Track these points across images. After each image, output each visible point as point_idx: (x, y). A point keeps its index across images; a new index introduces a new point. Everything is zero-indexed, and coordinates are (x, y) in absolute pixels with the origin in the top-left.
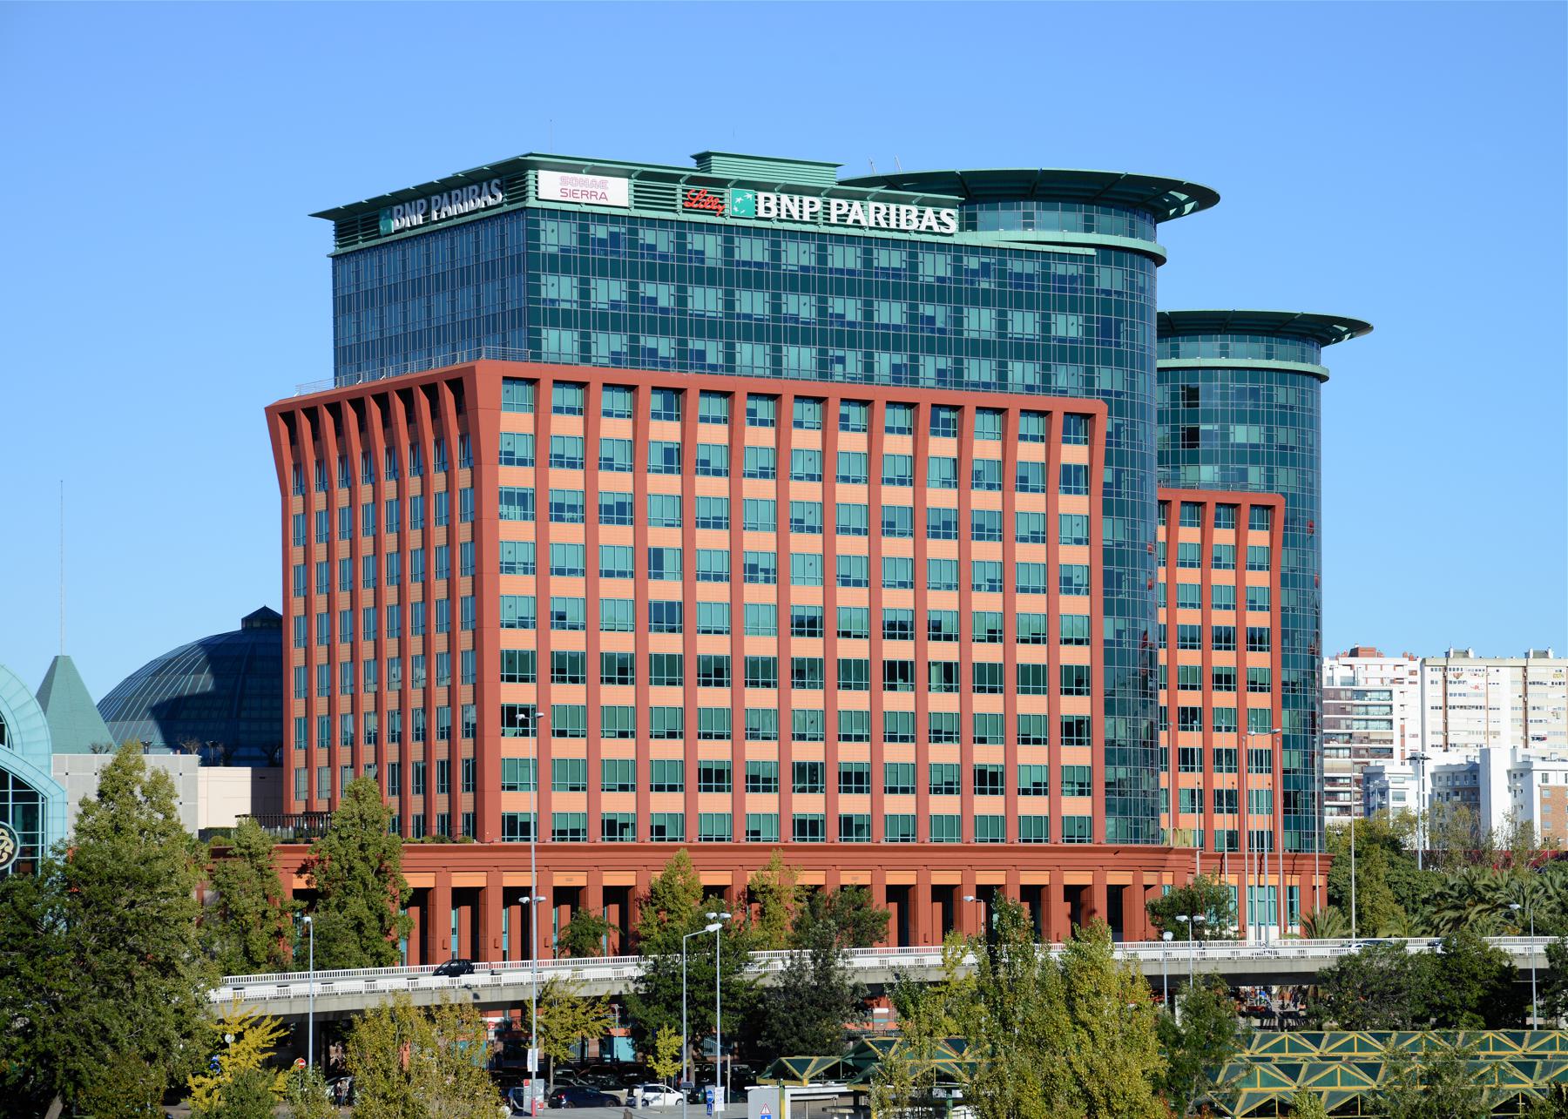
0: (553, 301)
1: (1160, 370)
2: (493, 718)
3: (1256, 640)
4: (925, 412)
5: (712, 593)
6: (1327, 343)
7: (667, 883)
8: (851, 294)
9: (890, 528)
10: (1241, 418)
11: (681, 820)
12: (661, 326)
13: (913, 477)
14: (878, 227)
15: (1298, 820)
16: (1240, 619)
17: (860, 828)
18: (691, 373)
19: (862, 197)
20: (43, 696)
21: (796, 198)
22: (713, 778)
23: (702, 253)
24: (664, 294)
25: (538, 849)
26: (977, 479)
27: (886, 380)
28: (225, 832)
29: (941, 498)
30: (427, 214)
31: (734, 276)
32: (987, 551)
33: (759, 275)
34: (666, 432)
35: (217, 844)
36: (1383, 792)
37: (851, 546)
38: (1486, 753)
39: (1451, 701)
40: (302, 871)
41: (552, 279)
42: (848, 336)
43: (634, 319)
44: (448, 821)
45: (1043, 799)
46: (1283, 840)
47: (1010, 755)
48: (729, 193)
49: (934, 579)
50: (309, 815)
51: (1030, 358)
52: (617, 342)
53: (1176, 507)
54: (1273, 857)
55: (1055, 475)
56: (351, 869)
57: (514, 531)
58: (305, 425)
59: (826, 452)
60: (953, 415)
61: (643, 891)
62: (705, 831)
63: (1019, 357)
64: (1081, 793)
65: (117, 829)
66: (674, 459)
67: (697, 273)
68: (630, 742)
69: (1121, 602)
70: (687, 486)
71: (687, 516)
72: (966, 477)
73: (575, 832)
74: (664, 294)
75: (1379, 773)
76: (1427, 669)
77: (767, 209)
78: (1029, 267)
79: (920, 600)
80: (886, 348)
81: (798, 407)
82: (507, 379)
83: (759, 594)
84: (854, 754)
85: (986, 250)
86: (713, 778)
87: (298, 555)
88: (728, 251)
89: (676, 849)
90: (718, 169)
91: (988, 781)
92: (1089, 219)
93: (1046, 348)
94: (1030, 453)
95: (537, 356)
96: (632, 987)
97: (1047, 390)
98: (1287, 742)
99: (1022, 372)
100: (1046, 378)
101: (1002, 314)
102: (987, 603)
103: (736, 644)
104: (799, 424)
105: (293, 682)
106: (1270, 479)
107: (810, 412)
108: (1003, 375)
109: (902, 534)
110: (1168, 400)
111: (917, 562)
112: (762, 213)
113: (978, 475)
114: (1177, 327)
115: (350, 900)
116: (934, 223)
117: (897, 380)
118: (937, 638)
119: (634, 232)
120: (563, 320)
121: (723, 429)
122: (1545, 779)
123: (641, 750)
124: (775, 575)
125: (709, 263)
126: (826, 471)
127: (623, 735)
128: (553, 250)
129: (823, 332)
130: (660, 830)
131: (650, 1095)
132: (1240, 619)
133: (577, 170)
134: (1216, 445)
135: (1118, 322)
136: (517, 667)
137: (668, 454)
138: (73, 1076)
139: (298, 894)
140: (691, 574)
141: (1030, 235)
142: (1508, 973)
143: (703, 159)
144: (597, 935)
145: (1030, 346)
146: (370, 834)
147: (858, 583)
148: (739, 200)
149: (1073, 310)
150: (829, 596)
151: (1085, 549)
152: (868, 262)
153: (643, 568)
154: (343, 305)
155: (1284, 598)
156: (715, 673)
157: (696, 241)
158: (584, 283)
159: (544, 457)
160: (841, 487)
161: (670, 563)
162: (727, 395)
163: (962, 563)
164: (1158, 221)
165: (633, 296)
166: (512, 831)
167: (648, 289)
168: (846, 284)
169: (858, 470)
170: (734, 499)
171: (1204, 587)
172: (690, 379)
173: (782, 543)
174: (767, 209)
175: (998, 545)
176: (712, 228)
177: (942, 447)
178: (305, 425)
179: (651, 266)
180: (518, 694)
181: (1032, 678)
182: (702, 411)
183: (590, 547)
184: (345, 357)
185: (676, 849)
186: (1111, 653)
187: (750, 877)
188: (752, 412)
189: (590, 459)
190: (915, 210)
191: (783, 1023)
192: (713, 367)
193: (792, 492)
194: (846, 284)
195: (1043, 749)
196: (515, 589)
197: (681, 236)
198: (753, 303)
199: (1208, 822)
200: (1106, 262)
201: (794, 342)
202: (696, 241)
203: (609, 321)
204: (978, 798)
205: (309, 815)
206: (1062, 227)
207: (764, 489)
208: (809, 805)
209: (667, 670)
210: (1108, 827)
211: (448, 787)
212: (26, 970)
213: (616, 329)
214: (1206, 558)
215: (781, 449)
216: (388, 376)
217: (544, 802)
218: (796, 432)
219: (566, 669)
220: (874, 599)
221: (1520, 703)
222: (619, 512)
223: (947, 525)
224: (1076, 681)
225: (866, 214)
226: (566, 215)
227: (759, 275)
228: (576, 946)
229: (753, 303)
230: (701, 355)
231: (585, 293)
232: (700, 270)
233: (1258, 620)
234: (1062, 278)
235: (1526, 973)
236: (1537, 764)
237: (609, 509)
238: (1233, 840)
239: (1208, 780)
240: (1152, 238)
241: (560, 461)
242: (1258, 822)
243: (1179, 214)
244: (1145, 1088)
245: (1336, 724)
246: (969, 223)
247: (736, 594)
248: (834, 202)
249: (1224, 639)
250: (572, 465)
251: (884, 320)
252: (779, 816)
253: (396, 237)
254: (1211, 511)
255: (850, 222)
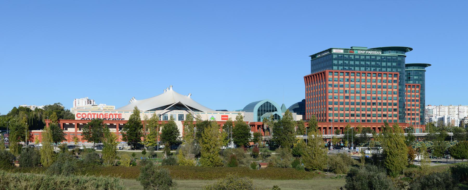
0: (334, 63)
1: (406, 70)
2: (328, 109)
3: (417, 101)
4: (377, 74)
5: (352, 95)
6: (426, 67)
7: (347, 127)
8: (369, 61)
9: (373, 87)
10: (415, 76)
11: (349, 120)
12: (347, 65)
13: (376, 81)
15: (422, 121)
16: (415, 98)
17: (369, 121)
18: (350, 71)
19: (370, 51)
20: (281, 108)
22: (352, 115)
23: (351, 57)
24: (347, 62)
25: (332, 123)
26: (384, 82)
27: (373, 71)
28: (299, 121)
29: (379, 84)
30: (321, 55)
31: (355, 60)
32: (385, 90)
33: (358, 60)
34: (347, 77)
35: (298, 122)
36: (432, 121)
38: (444, 116)
39: (440, 111)
40: (307, 125)
41: (334, 61)
42: (368, 66)
43: (344, 65)
44: (323, 120)
45: (391, 118)
46: (420, 123)
47: (387, 113)
48: (354, 51)
49: (378, 93)
50: (308, 119)
51: (390, 68)
52: (342, 68)
53: (407, 86)
54: (419, 125)
55: (393, 81)
56: (312, 125)
57: (330, 88)
58: (308, 78)
59: (366, 79)
60: (381, 75)
61: (344, 128)
62: (351, 121)
63: (389, 68)
64: (396, 117)
65: (287, 118)
66: (348, 80)
67: (350, 59)
68: (343, 111)
69: (401, 95)
70: (350, 83)
71: (350, 86)
72: (382, 81)
73: (337, 121)
74: (347, 62)
75: (431, 119)
76: (437, 107)
78: (390, 58)
79: (377, 95)
80: (373, 67)
81: (362, 74)
82: (329, 72)
83: (358, 95)
84: (369, 113)
85: (385, 56)
86: (352, 115)
88: (354, 57)
89: (348, 123)
90: (353, 48)
91: (385, 116)
92: (397, 52)
93: (392, 67)
94: (390, 79)
95: (333, 69)
96: (343, 137)
97: (392, 71)
98: (421, 112)
99: (389, 70)
100: (392, 70)
101: (387, 63)
102: (385, 96)
103: (355, 101)
104: (363, 76)
105: (306, 106)
106: (419, 82)
107: (364, 75)
108: (387, 70)
109: (375, 88)
110: (406, 78)
111: (376, 91)
112: (358, 53)
113: (384, 81)
114: (408, 66)
115: (312, 128)
117: (374, 71)
118: (379, 100)
119: (344, 55)
120: (335, 65)
121: (354, 77)
122: (451, 119)
123: (344, 112)
124: (360, 93)
125: (352, 59)
126: (366, 81)
128: (335, 58)
129: (365, 66)
130: (346, 121)
131: (345, 148)
132: (415, 98)
134: (412, 79)
135: (401, 64)
136: (331, 103)
137: (347, 80)
138: (282, 143)
139: (307, 127)
140: (350, 93)
141: (390, 54)
142: (448, 136)
143: (352, 47)
144: (339, 132)
145: (390, 66)
146: (314, 121)
147: (369, 94)
149: (395, 62)
150: (366, 95)
151: (396, 89)
152: (371, 58)
153: (344, 92)
155: (420, 96)
156: (353, 104)
157: (351, 56)
158: (338, 61)
159: (333, 80)
160: (367, 83)
161: (348, 92)
162: (354, 73)
163: (382, 91)
164: (405, 52)
165: (344, 62)
166: (330, 121)
167: (345, 62)
168: (368, 60)
169: (369, 81)
170: (355, 85)
171: (411, 95)
172: (350, 71)
173: (360, 89)
175: (386, 89)
176: (353, 55)
177: (379, 78)
178: (308, 78)
179: (346, 59)
181: (390, 104)
182: (351, 75)
183: (339, 90)
184: (312, 71)
185: (348, 123)
186: (400, 101)
187: (357, 126)
188: (357, 75)
189: (339, 80)
190: (376, 52)
191: (360, 141)
192: (353, 70)
194: (368, 60)
195: (391, 112)
196: (330, 95)
197: (349, 56)
198: (357, 63)
199: (411, 121)
200: (399, 57)
201: (362, 67)
203: (341, 65)
204: (383, 118)
205: (308, 119)
206: (394, 53)
207: (358, 83)
208: (363, 118)
209: (348, 103)
210: (399, 121)
211: (323, 116)
212: (277, 132)
213: (342, 66)
214: (411, 92)
215: (360, 79)
216: (317, 72)
217: (333, 118)
218: (362, 77)
219: (336, 104)
220: (371, 95)
221: (448, 111)
222: (342, 86)
223: (380, 87)
224: (395, 105)
225: (370, 52)
226: (336, 54)
227: (358, 60)
228: (337, 133)
229: (357, 63)
230: (351, 69)
231: (338, 62)
232: (351, 59)
233: (417, 98)
234: (394, 59)
235: (451, 136)
236: (450, 117)
237: (341, 86)
238: (414, 123)
239: (411, 117)
240: (405, 54)
241: (335, 81)
242: (417, 121)
243: (408, 51)
244: (403, 143)
245: (426, 113)
246: (383, 53)
247: (355, 95)
248: (367, 51)
249: (413, 100)
250: (337, 81)
251: (373, 64)
252: (360, 120)
254: (412, 86)
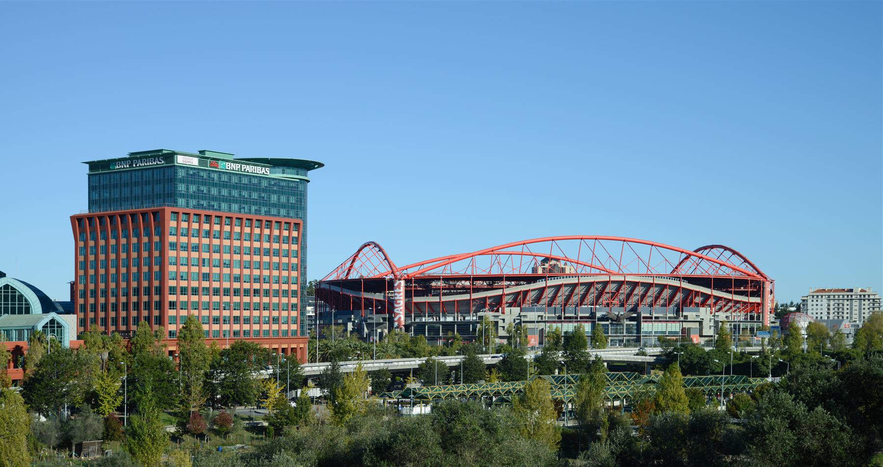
5: (216, 270)
14: (233, 170)
21: (235, 164)
24: (204, 189)
29: (266, 245)
34: (206, 227)
37: (247, 258)
48: (220, 162)
74: (204, 189)
77: (228, 167)
78: (285, 184)
87: (81, 258)
91: (276, 320)
100: (288, 214)
108: (279, 213)
112: (227, 168)
116: (264, 172)
119: (199, 172)
120: (183, 196)
127: (195, 309)
133: (186, 156)
141: (285, 175)
148: (222, 164)
154: (91, 188)
156: (217, 292)
157: (212, 175)
167: (202, 188)
174: (228, 167)
180: (172, 298)
184: (91, 203)
192: (216, 209)
193: (244, 244)
202: (212, 175)
203: (193, 197)
208: (236, 327)
248: (243, 165)
253: (117, 170)
255: (246, 171)
